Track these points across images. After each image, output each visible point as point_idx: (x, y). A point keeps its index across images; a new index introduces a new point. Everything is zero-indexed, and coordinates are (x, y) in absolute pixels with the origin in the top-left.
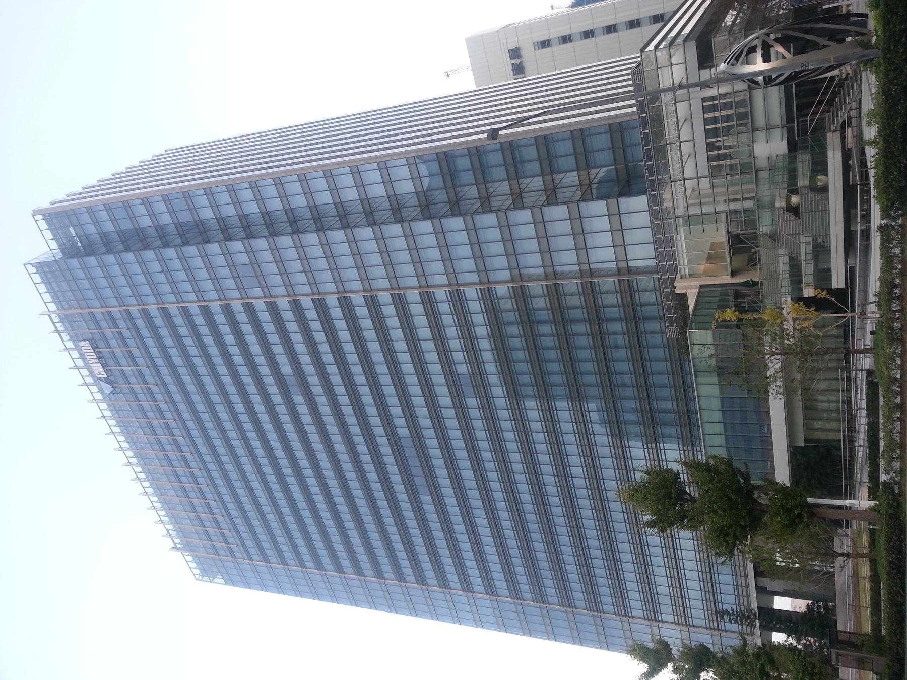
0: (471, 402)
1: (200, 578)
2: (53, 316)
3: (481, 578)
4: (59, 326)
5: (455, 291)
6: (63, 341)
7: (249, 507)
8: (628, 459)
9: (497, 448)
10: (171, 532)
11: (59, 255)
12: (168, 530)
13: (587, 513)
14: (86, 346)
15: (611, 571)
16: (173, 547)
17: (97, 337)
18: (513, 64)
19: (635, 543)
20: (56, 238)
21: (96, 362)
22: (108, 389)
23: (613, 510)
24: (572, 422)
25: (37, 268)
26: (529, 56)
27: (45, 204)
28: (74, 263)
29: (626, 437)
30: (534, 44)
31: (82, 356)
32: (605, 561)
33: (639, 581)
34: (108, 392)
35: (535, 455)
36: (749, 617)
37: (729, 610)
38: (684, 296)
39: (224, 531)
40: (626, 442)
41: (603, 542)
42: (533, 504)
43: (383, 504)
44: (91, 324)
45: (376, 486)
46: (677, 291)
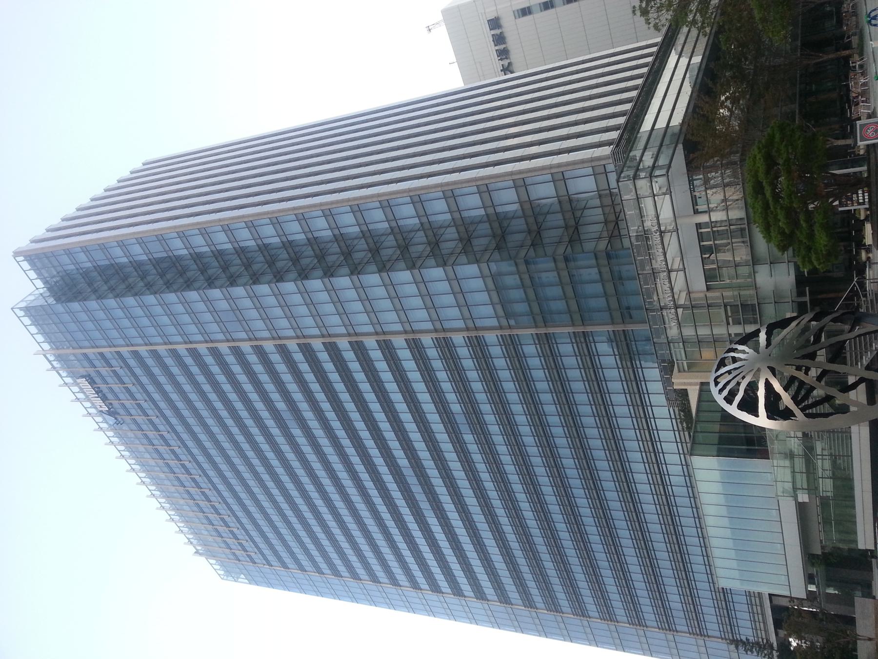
2: (48, 356)
3: (464, 471)
4: (55, 363)
5: (474, 338)
6: (62, 377)
7: (218, 460)
8: (640, 381)
9: (516, 452)
13: (574, 374)
15: (601, 418)
16: (195, 552)
17: (93, 374)
18: (493, 35)
19: (644, 439)
20: (40, 276)
21: (96, 397)
22: (111, 420)
23: (605, 367)
24: (576, 356)
25: (25, 311)
26: (510, 25)
27: (23, 242)
29: (636, 357)
30: (514, 12)
31: (82, 391)
32: (607, 452)
33: (646, 461)
34: (111, 423)
35: (548, 428)
39: (115, 369)
40: (638, 362)
41: (606, 442)
42: (522, 404)
44: (86, 364)
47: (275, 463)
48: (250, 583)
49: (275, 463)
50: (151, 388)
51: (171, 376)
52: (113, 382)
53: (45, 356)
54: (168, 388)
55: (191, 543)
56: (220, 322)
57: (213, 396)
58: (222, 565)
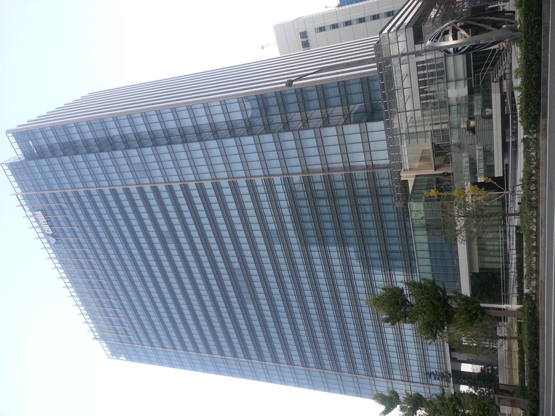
0: (278, 247)
1: (111, 357)
2: (19, 196)
6: (25, 211)
10: (93, 329)
11: (23, 158)
12: (91, 327)
14: (39, 214)
16: (94, 338)
18: (302, 42)
22: (53, 241)
28: (32, 163)
29: (371, 268)
31: (37, 221)
34: (53, 243)
36: (446, 376)
37: (434, 372)
38: (406, 182)
39: (130, 336)
40: (372, 271)
43: (224, 310)
45: (220, 299)
46: (402, 179)
47: (155, 269)
48: (127, 360)
49: (155, 269)
50: (125, 303)
51: (117, 250)
52: (97, 287)
53: (17, 196)
54: (121, 273)
55: (92, 331)
56: (133, 171)
57: (122, 223)
58: (110, 346)
